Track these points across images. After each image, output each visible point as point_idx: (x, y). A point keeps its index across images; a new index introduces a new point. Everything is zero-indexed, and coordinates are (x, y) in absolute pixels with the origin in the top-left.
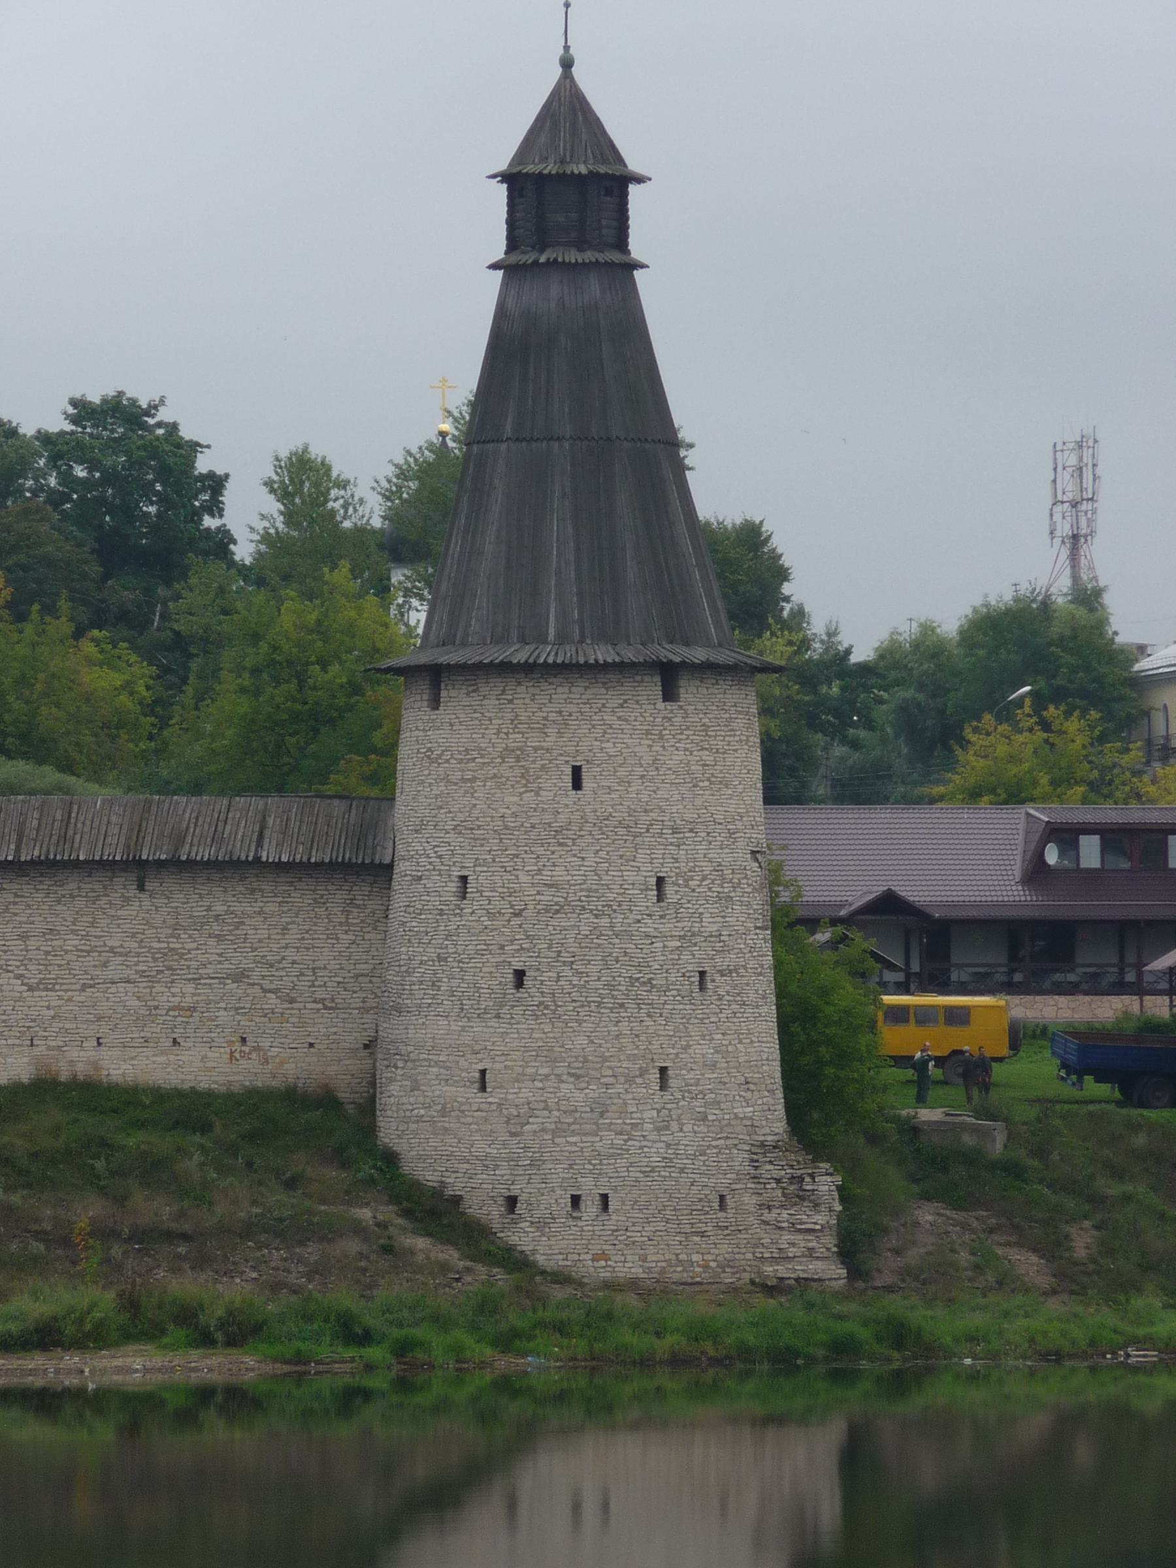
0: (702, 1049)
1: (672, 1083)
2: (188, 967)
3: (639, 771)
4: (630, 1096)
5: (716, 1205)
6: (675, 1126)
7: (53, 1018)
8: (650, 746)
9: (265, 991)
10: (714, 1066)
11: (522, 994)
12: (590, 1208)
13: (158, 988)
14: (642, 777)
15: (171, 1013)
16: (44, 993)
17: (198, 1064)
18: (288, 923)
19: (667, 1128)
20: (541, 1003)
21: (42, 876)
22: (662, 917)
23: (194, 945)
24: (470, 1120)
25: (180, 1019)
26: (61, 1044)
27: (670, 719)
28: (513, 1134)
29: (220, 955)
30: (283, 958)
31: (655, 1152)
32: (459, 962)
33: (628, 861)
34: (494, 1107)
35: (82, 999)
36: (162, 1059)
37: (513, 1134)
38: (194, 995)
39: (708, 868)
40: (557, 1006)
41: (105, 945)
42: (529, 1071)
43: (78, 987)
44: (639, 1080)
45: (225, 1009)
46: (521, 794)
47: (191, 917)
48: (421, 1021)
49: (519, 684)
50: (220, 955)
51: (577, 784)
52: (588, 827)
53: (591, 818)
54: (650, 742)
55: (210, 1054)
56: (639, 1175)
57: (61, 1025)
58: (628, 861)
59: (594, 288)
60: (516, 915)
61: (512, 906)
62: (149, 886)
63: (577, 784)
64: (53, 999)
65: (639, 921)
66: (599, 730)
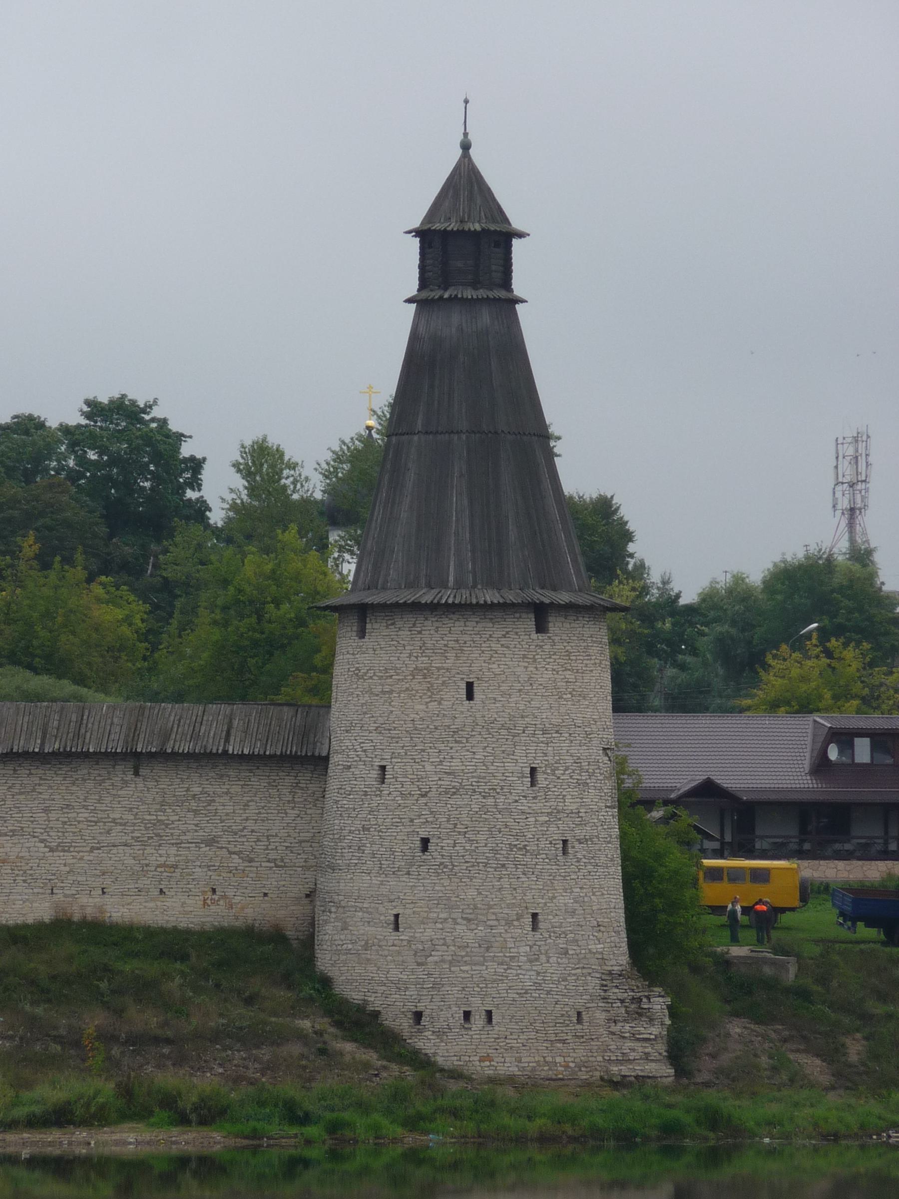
0: (565, 900)
1: (541, 925)
2: (172, 834)
3: (518, 686)
5: (575, 1020)
6: (543, 958)
8: (526, 667)
9: (231, 853)
12: (478, 1021)
13: (149, 850)
14: (520, 690)
15: (159, 869)
16: (62, 854)
18: (249, 801)
19: (537, 960)
20: (442, 863)
21: (60, 764)
22: (534, 798)
23: (177, 818)
24: (386, 953)
25: (165, 874)
26: (74, 892)
27: (541, 647)
28: (419, 964)
29: (196, 825)
30: (244, 828)
33: (508, 755)
34: (405, 943)
35: (91, 858)
36: (151, 905)
37: (419, 964)
38: (177, 855)
39: (570, 761)
40: (454, 866)
41: (109, 817)
44: (515, 923)
45: (200, 866)
46: (427, 703)
47: (174, 796)
49: (426, 619)
50: (196, 825)
51: (470, 696)
52: (478, 728)
53: (480, 721)
54: (526, 664)
55: (189, 902)
56: (515, 995)
57: (75, 878)
58: (508, 755)
59: (485, 318)
61: (420, 789)
62: (142, 772)
63: (470, 696)
65: (516, 801)
66: (487, 655)
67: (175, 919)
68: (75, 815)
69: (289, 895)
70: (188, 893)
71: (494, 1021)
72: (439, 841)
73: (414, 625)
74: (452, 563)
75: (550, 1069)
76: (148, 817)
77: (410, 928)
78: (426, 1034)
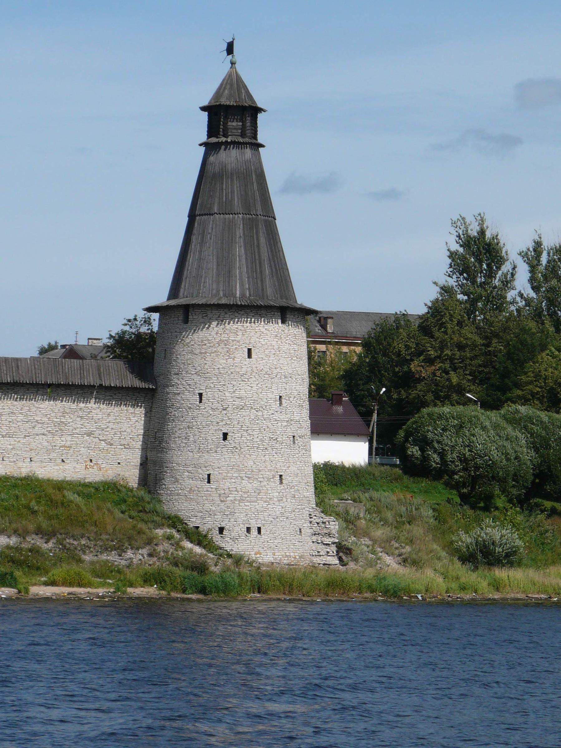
0: (293, 469)
1: (284, 481)
2: (69, 430)
3: (273, 352)
4: (269, 486)
6: (284, 500)
7: (12, 449)
8: (277, 342)
9: (100, 440)
10: (297, 475)
11: (226, 442)
12: (254, 532)
13: (56, 438)
14: (274, 354)
15: (61, 448)
16: (8, 439)
17: (72, 470)
18: (110, 412)
19: (282, 500)
20: (235, 447)
21: (8, 389)
22: (281, 412)
23: (71, 420)
24: (203, 495)
27: (283, 331)
28: (222, 501)
29: (82, 425)
30: (108, 427)
31: (278, 510)
32: (199, 429)
33: (269, 389)
34: (214, 490)
35: (24, 441)
37: (222, 501)
38: (71, 441)
39: (296, 393)
40: (241, 448)
41: (34, 419)
42: (229, 475)
43: (23, 436)
44: (272, 480)
46: (227, 359)
47: (70, 408)
48: (179, 453)
49: (226, 313)
50: (82, 425)
51: (250, 356)
52: (254, 374)
53: (255, 370)
54: (277, 340)
55: (77, 466)
56: (272, 519)
57: (15, 452)
58: (269, 389)
59: (248, 153)
60: (224, 410)
61: (222, 406)
63: (250, 356)
64: (12, 440)
65: (273, 414)
66: (258, 334)
67: (69, 475)
68: (16, 418)
69: (132, 464)
70: (77, 462)
71: (262, 533)
72: (233, 434)
73: (219, 317)
74: (238, 284)
75: (288, 560)
76: (55, 420)
77: (217, 481)
78: (226, 539)
